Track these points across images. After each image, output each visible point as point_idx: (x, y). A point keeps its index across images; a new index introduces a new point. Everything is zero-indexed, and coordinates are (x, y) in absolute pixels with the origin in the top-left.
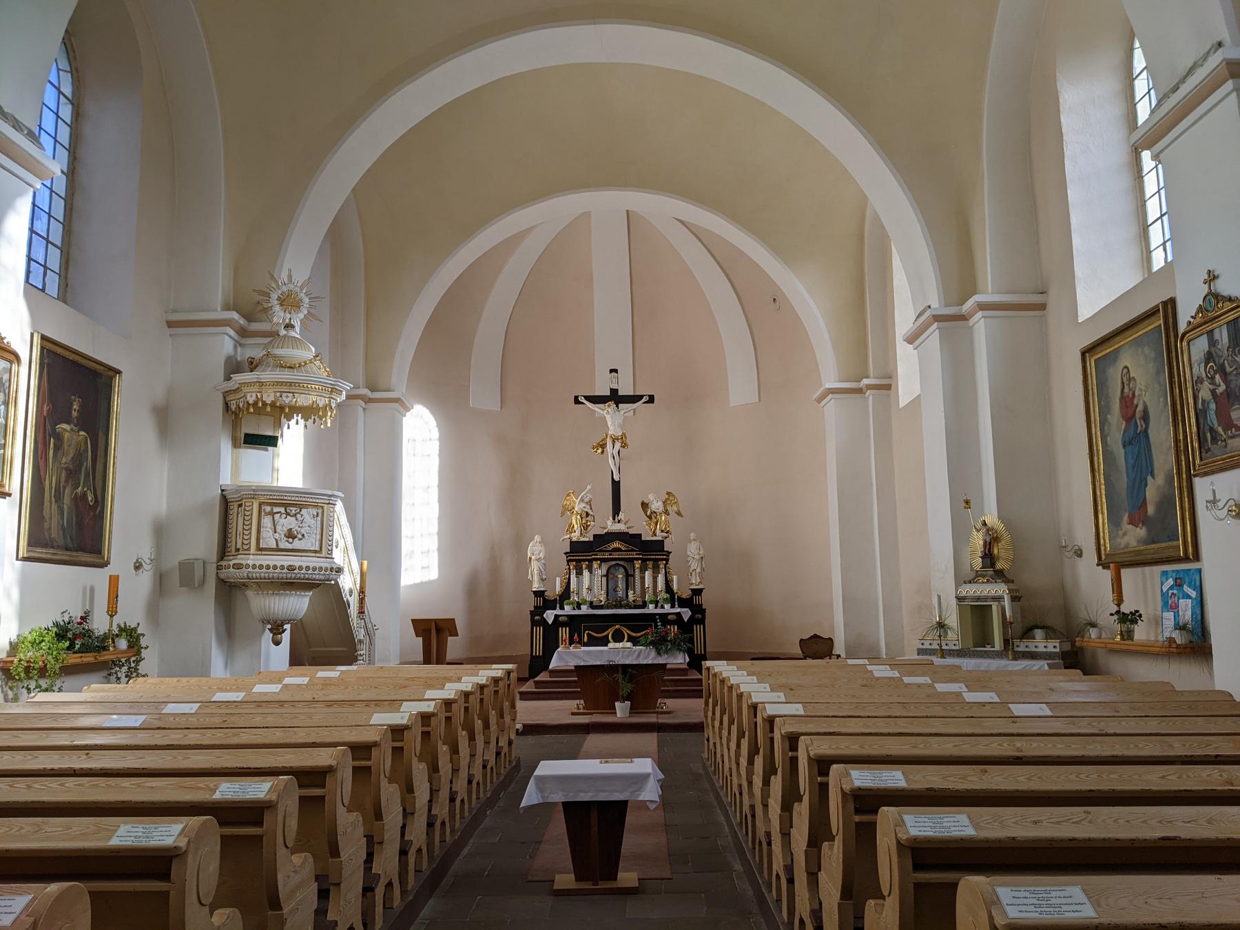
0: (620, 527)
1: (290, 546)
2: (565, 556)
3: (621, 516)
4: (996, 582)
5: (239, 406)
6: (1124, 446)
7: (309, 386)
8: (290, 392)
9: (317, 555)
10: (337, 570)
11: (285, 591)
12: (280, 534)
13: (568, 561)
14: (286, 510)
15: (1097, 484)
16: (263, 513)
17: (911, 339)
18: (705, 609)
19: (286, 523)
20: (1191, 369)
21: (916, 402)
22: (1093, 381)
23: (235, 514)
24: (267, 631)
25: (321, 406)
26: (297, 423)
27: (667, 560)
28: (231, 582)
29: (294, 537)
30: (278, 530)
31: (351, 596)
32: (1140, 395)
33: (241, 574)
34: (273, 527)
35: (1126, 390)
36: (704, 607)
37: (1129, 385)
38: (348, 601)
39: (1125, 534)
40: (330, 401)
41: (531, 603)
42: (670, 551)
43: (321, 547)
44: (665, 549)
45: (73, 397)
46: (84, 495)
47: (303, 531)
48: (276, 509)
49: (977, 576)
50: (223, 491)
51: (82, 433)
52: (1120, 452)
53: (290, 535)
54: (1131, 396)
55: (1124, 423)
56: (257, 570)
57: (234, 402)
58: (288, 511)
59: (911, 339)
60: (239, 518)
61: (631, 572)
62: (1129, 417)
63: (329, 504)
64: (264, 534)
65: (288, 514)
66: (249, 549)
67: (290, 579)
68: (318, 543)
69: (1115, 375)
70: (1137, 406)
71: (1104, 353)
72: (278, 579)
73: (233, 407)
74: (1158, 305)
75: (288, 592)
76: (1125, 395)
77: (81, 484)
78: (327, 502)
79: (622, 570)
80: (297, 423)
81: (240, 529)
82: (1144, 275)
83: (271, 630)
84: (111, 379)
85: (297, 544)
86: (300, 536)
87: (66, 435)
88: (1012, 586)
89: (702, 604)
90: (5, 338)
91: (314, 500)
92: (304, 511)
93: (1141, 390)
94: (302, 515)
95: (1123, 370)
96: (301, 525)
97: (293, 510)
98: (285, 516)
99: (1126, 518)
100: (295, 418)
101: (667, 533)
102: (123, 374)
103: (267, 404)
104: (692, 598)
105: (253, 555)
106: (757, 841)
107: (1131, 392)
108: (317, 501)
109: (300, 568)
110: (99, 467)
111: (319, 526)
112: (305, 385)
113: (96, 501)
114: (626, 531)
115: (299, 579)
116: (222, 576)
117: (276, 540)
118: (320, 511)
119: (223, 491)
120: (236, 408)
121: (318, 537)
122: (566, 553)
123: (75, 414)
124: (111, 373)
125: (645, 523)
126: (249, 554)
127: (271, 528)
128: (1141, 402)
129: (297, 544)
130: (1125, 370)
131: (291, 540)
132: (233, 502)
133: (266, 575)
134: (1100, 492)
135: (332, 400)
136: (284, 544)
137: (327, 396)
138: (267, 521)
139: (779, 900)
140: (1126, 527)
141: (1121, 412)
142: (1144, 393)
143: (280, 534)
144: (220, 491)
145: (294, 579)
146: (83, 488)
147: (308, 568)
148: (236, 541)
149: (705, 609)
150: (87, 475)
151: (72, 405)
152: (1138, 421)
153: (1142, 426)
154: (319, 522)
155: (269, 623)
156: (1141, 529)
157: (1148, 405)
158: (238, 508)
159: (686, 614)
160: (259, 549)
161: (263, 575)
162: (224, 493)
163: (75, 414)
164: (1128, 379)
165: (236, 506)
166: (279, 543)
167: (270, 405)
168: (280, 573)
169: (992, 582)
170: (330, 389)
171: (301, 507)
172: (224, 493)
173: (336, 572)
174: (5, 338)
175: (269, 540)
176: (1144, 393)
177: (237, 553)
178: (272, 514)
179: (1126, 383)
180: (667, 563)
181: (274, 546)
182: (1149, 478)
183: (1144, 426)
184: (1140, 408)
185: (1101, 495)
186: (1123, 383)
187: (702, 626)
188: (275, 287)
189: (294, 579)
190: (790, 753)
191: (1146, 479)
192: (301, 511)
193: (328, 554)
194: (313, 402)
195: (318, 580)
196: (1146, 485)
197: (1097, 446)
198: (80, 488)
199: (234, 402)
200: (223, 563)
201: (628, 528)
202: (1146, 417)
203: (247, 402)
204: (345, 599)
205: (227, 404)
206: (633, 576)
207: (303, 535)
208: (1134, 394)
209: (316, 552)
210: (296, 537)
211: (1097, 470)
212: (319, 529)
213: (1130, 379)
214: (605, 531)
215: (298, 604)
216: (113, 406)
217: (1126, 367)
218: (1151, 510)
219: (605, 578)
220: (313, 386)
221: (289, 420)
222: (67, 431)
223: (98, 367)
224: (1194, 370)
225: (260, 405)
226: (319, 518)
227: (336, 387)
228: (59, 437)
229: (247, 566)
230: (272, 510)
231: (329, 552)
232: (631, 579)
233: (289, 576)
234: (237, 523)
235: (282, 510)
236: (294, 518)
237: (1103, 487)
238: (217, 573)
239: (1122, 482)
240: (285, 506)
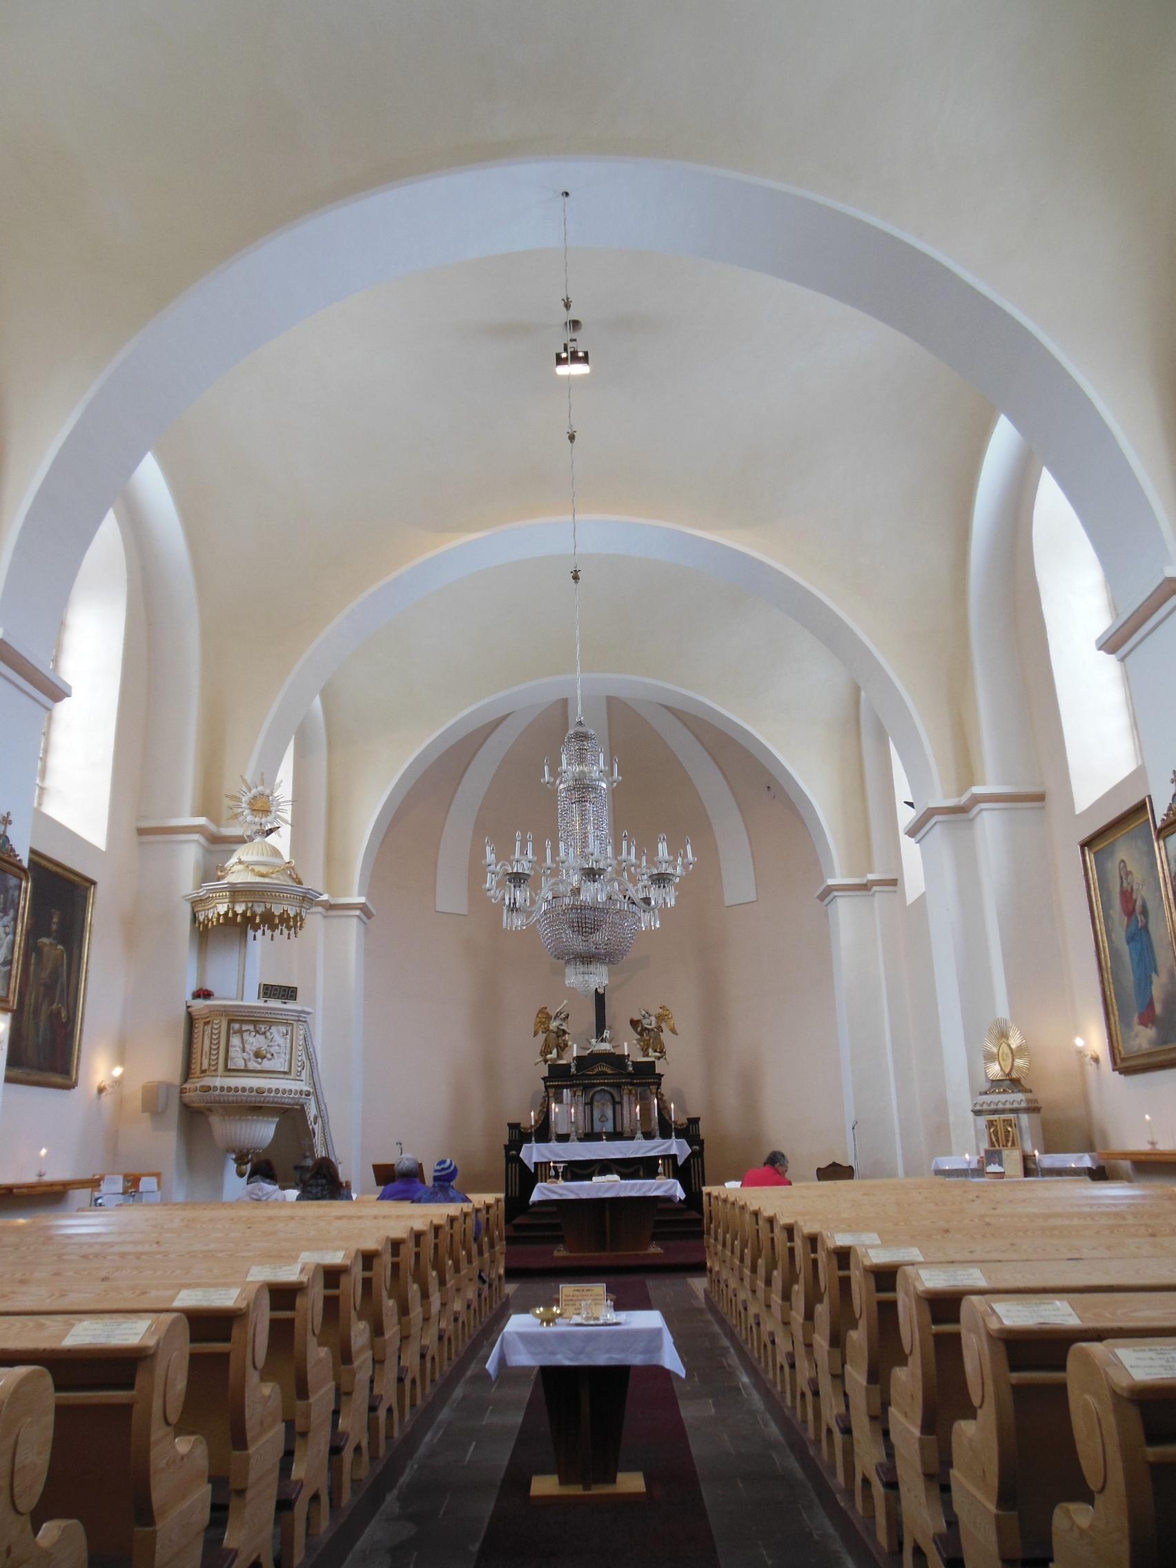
0: (605, 1047)
1: (259, 1067)
2: (543, 1082)
3: (606, 1034)
4: (1013, 1092)
5: (207, 916)
6: (1128, 943)
7: (281, 895)
8: (261, 902)
9: (287, 1076)
10: (307, 1093)
11: (246, 1116)
12: (249, 1054)
13: (546, 1087)
14: (255, 1028)
15: (1106, 984)
16: (231, 1031)
17: (912, 832)
18: (703, 1140)
19: (255, 1042)
20: (1169, 865)
21: (922, 898)
22: (1093, 875)
23: (201, 1033)
24: (232, 1162)
25: (292, 915)
26: (264, 934)
27: (659, 1084)
28: (192, 1107)
29: (263, 1057)
30: (247, 1050)
31: (315, 1124)
32: (1138, 890)
33: (208, 1098)
34: (241, 1046)
35: (1125, 885)
36: (701, 1138)
37: (1126, 879)
38: (313, 1129)
39: (1137, 1035)
40: (301, 910)
41: (504, 1137)
42: (662, 1073)
43: (290, 1069)
44: (657, 1072)
45: (53, 910)
46: (59, 1013)
47: (272, 1050)
48: (245, 1027)
49: (992, 1087)
50: (188, 1007)
51: (60, 947)
52: (1124, 948)
53: (258, 1055)
54: (1129, 890)
55: (1126, 918)
56: (225, 1093)
57: (203, 913)
58: (257, 1029)
59: (912, 832)
60: (206, 1037)
61: (617, 1099)
62: (1129, 911)
63: (299, 1020)
64: (232, 1053)
65: (257, 1032)
66: (216, 1070)
67: (260, 1102)
68: (287, 1063)
69: (1113, 867)
70: (1136, 901)
71: (1102, 846)
72: (246, 1102)
73: (201, 918)
74: (1144, 800)
75: (255, 1118)
76: (1125, 889)
77: (57, 1000)
78: (297, 1018)
79: (608, 1096)
80: (264, 934)
81: (206, 1048)
82: (1137, 763)
83: (236, 1160)
84: (87, 889)
85: (267, 1065)
86: (269, 1056)
87: (46, 949)
88: (1029, 1096)
89: (699, 1135)
90: (18, 855)
91: (284, 1017)
92: (274, 1029)
93: (1138, 884)
94: (271, 1033)
95: (1120, 864)
96: (271, 1044)
97: (263, 1028)
98: (254, 1033)
99: (1136, 1019)
100: (262, 928)
101: (660, 1052)
102: (99, 886)
103: (237, 915)
104: (688, 1127)
105: (221, 1076)
106: (763, 1344)
107: (1129, 887)
108: (286, 1017)
109: (270, 1090)
110: (73, 982)
111: (288, 1045)
112: (277, 894)
113: (68, 1018)
114: (612, 1051)
115: (268, 1102)
116: (186, 1100)
117: (245, 1060)
118: (289, 1029)
119: (188, 1007)
120: (204, 920)
121: (288, 1057)
122: (544, 1079)
123: (54, 927)
124: (87, 884)
125: (635, 1042)
126: (217, 1076)
127: (240, 1047)
128: (1139, 896)
129: (267, 1065)
130: (1122, 864)
131: (259, 1060)
132: (198, 1019)
133: (235, 1098)
134: (1110, 992)
135: (303, 909)
136: (253, 1065)
137: (298, 905)
138: (235, 1041)
139: (783, 1392)
140: (1139, 1028)
141: (1123, 907)
142: (1141, 887)
143: (249, 1054)
144: (185, 1008)
145: (263, 1103)
146: (58, 1005)
147: (277, 1090)
148: (202, 1060)
149: (703, 1140)
150: (62, 991)
151: (52, 918)
152: (1139, 917)
153: (1142, 921)
154: (288, 1041)
155: (234, 1151)
156: (1151, 1029)
157: (1147, 901)
158: (204, 1026)
159: (678, 1147)
160: (227, 1069)
161: (231, 1098)
162: (190, 1009)
163: (54, 927)
164: (1125, 874)
165: (202, 1025)
166: (248, 1063)
167: (278, 916)
168: (249, 1096)
169: (1008, 1093)
170: (301, 898)
171: (271, 1023)
172: (190, 1009)
173: (306, 1095)
174: (18, 855)
175: (238, 1061)
176: (1141, 887)
177: (203, 1075)
178: (240, 1032)
179: (1124, 877)
180: (658, 1088)
181: (243, 1068)
182: (1154, 975)
183: (1144, 921)
184: (1139, 903)
185: (1111, 995)
186: (1121, 878)
187: (700, 1160)
188: (247, 791)
189: (263, 1103)
190: (789, 1244)
191: (1150, 977)
192: (270, 1029)
193: (298, 1076)
194: (297, 913)
195: (287, 1104)
196: (1151, 983)
197: (1103, 943)
198: (55, 1004)
199: (203, 913)
200: (187, 1086)
201: (613, 1047)
202: (1145, 912)
203: (218, 913)
204: (311, 1127)
205: (195, 915)
206: (621, 1103)
207: (272, 1055)
208: (1132, 888)
209: (285, 1073)
210: (265, 1057)
211: (1105, 968)
212: (288, 1048)
213: (1128, 873)
214: (588, 1052)
215: (263, 1132)
216: (87, 918)
217: (1123, 861)
218: (1158, 1009)
219: (589, 1106)
220: (285, 895)
221: (256, 931)
222: (47, 945)
223: (76, 879)
224: (1171, 866)
225: (285, 916)
226: (288, 1037)
227: (311, 892)
228: (39, 951)
229: (215, 1088)
230: (241, 1028)
231: (299, 1074)
232: (618, 1107)
233: (258, 1099)
234: (204, 1042)
235: (251, 1027)
236: (263, 1037)
237: (1112, 986)
238: (181, 1097)
239: (1129, 978)
240: (255, 1023)
